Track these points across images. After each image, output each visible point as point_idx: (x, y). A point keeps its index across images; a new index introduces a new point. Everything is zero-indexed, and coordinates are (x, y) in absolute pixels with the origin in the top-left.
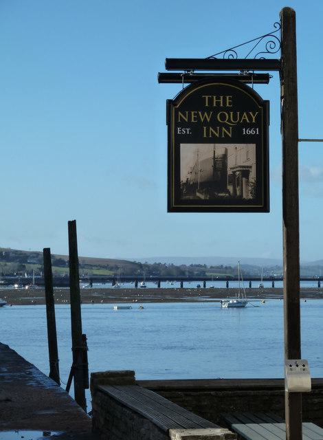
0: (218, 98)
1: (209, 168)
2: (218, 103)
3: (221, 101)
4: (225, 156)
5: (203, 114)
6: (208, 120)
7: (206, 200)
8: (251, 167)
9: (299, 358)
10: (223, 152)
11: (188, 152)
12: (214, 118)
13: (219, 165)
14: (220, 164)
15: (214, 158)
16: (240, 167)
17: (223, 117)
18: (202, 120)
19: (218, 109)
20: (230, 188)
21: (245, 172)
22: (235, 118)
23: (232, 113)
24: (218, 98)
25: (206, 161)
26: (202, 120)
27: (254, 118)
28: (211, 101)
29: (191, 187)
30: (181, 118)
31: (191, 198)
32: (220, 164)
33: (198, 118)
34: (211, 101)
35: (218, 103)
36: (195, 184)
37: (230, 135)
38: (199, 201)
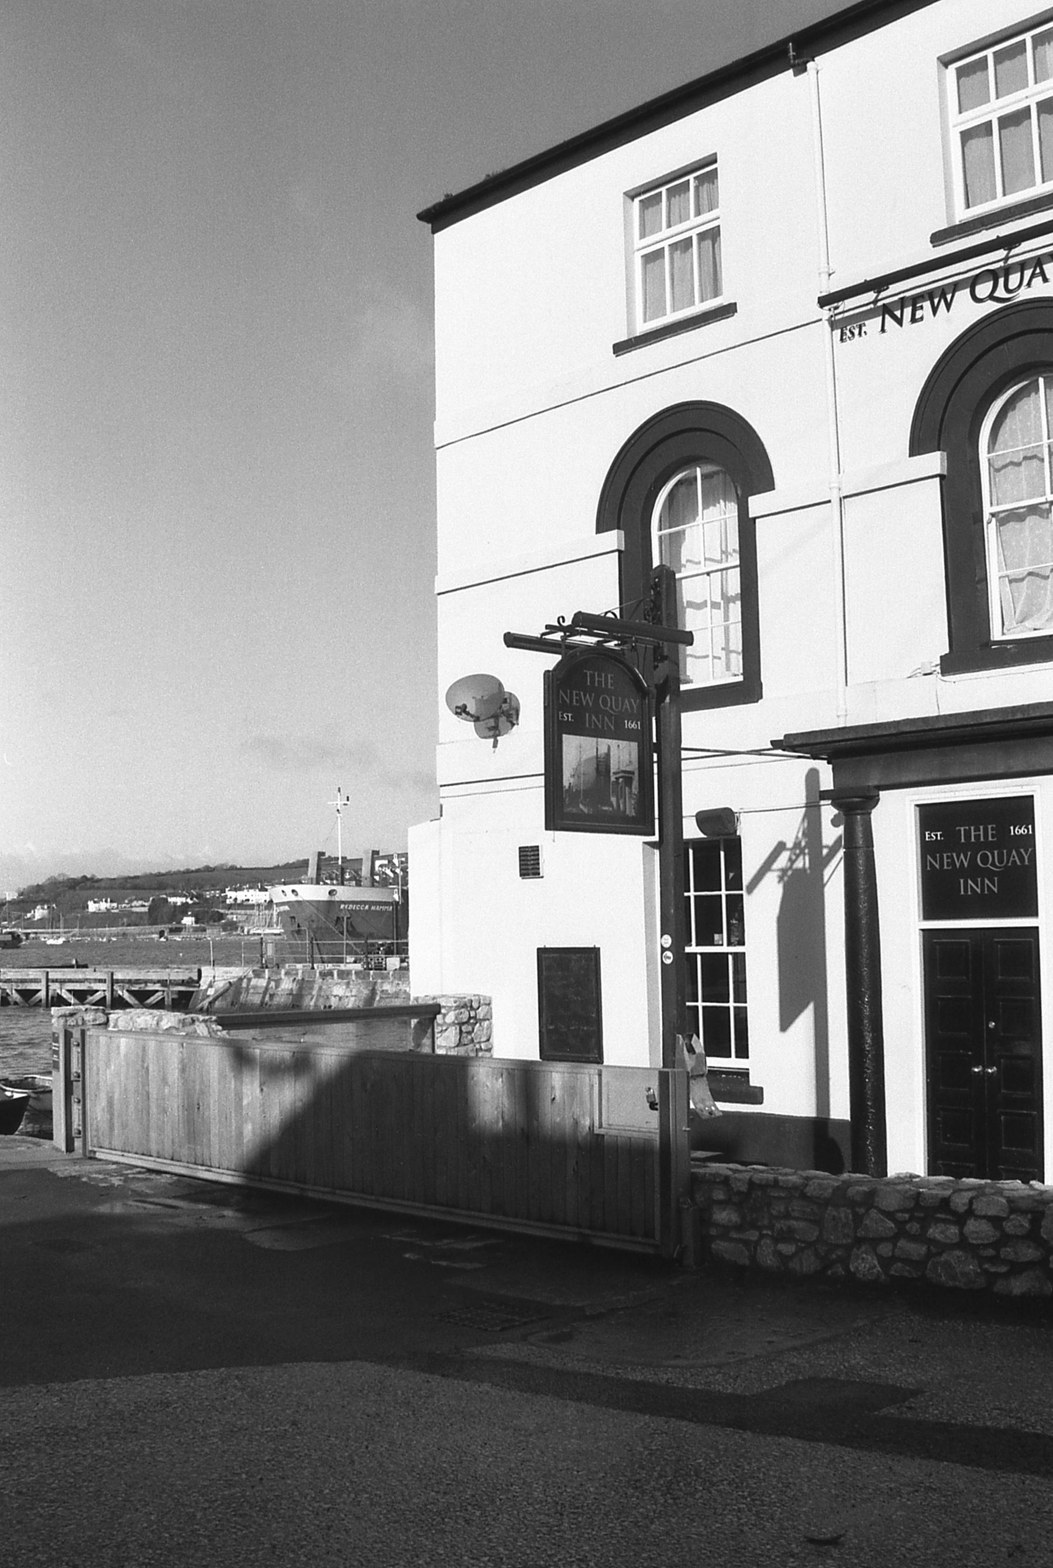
0: (977, 830)
1: (591, 769)
2: (977, 837)
3: (982, 833)
4: (608, 755)
5: (585, 696)
6: (966, 864)
7: (588, 815)
8: (633, 773)
9: (599, 1060)
10: (606, 751)
11: (577, 750)
12: (973, 861)
13: (602, 768)
14: (602, 764)
15: (597, 757)
16: (623, 772)
17: (605, 701)
18: (958, 865)
19: (978, 846)
20: (613, 799)
21: (628, 779)
22: (1001, 861)
23: (996, 852)
24: (977, 830)
25: (588, 760)
26: (958, 865)
27: (1026, 858)
28: (968, 834)
29: (574, 794)
30: (931, 865)
31: (574, 810)
32: (602, 764)
33: (579, 701)
34: (968, 834)
35: (977, 837)
36: (578, 791)
37: (996, 890)
38: (582, 817)
